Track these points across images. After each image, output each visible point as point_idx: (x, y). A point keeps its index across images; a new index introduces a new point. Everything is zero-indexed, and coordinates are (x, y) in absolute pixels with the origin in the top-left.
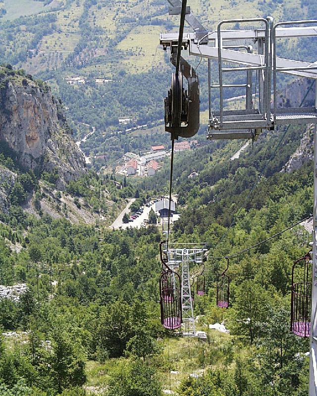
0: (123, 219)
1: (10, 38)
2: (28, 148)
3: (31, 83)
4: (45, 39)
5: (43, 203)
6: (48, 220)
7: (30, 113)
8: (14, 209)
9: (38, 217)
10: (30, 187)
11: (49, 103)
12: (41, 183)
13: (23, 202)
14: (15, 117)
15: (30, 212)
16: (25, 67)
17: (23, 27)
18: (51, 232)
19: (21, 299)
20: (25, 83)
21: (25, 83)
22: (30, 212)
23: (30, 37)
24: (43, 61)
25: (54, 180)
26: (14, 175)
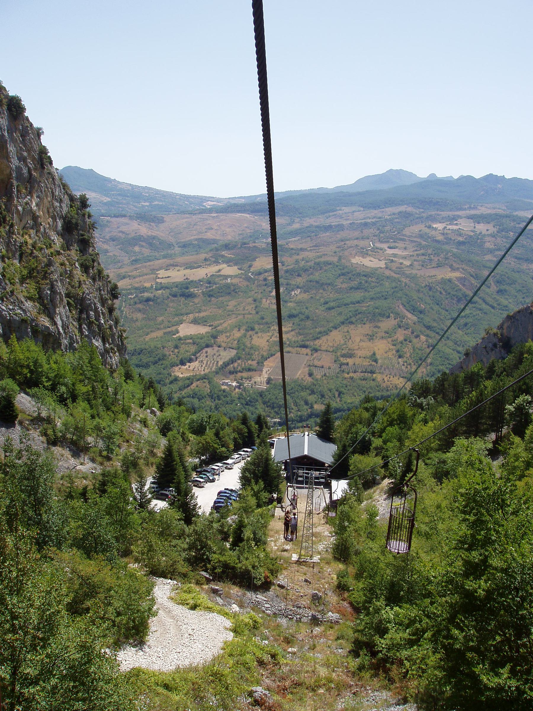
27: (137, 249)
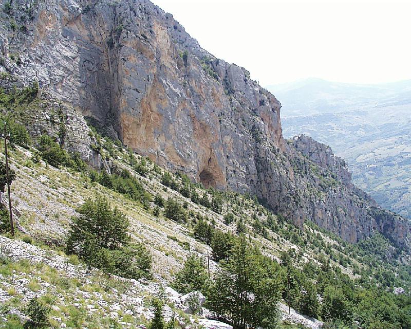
0: (195, 40)
1: (392, 194)
2: (399, 240)
3: (402, 219)
4: (404, 195)
5: (402, 258)
6: (404, 265)
7: (401, 228)
8: (393, 260)
9: (401, 264)
10: (399, 253)
11: (407, 225)
12: (402, 251)
13: (396, 258)
14: (396, 229)
15: (398, 261)
16: (400, 214)
17: (396, 191)
18: (405, 269)
19: (217, 260)
20: (400, 218)
21: (400, 218)
22: (398, 261)
23: (398, 194)
24: (403, 203)
25: (407, 251)
26: (394, 248)
27: (358, 132)
